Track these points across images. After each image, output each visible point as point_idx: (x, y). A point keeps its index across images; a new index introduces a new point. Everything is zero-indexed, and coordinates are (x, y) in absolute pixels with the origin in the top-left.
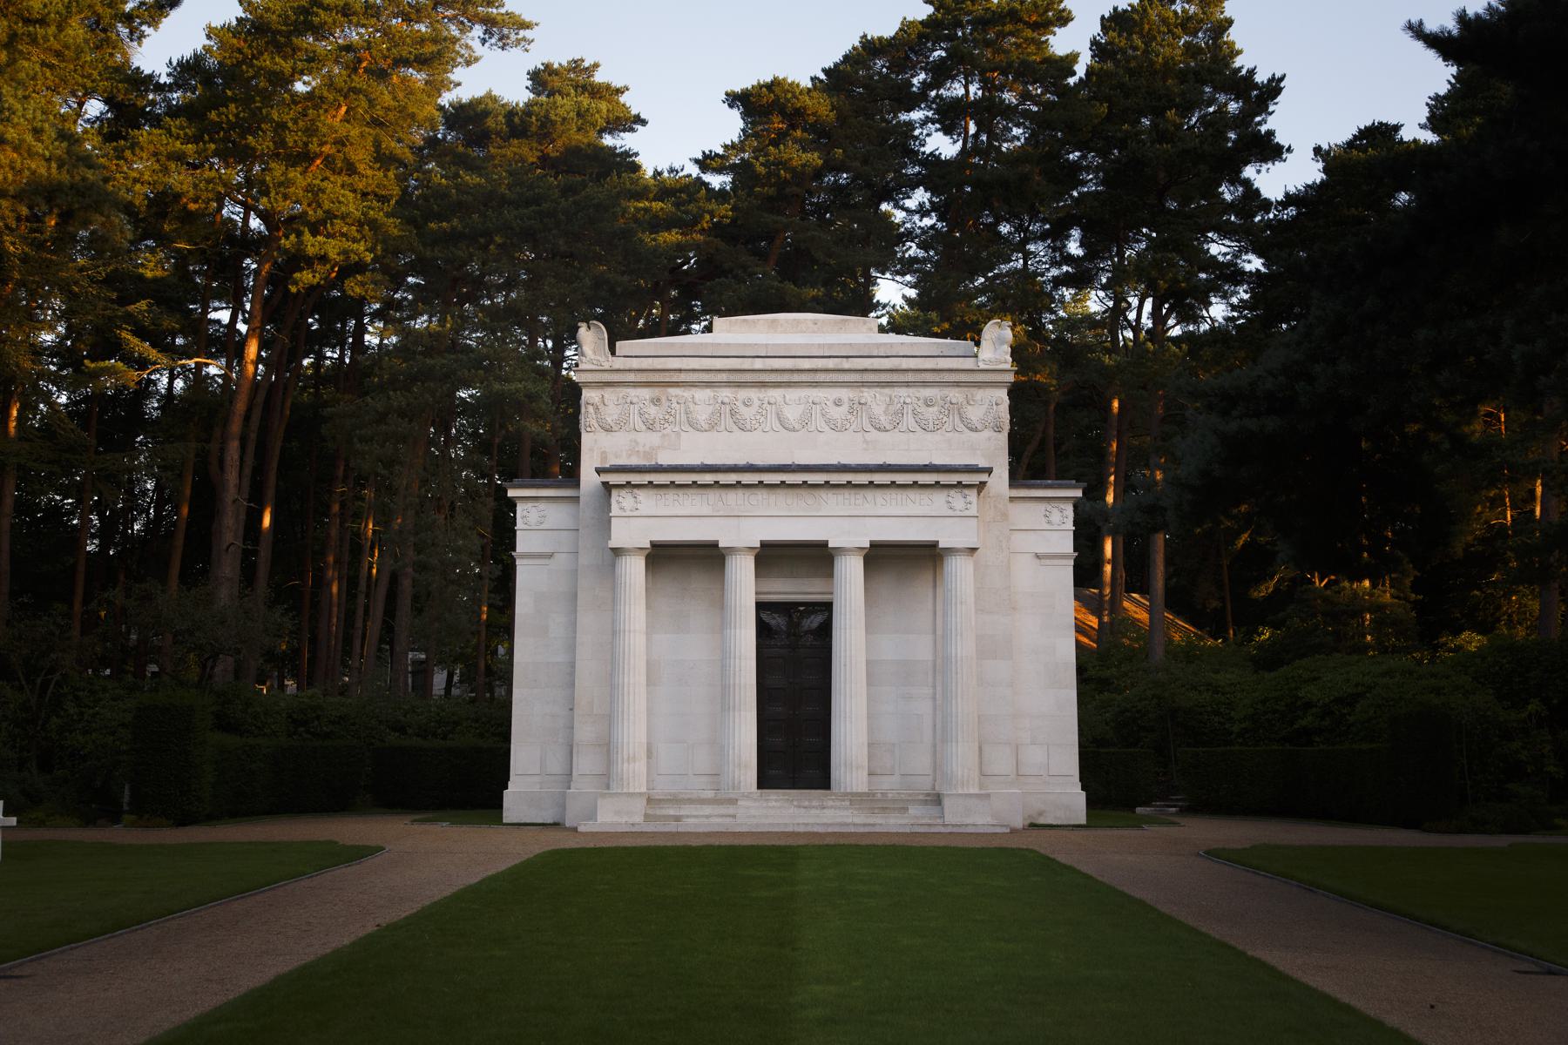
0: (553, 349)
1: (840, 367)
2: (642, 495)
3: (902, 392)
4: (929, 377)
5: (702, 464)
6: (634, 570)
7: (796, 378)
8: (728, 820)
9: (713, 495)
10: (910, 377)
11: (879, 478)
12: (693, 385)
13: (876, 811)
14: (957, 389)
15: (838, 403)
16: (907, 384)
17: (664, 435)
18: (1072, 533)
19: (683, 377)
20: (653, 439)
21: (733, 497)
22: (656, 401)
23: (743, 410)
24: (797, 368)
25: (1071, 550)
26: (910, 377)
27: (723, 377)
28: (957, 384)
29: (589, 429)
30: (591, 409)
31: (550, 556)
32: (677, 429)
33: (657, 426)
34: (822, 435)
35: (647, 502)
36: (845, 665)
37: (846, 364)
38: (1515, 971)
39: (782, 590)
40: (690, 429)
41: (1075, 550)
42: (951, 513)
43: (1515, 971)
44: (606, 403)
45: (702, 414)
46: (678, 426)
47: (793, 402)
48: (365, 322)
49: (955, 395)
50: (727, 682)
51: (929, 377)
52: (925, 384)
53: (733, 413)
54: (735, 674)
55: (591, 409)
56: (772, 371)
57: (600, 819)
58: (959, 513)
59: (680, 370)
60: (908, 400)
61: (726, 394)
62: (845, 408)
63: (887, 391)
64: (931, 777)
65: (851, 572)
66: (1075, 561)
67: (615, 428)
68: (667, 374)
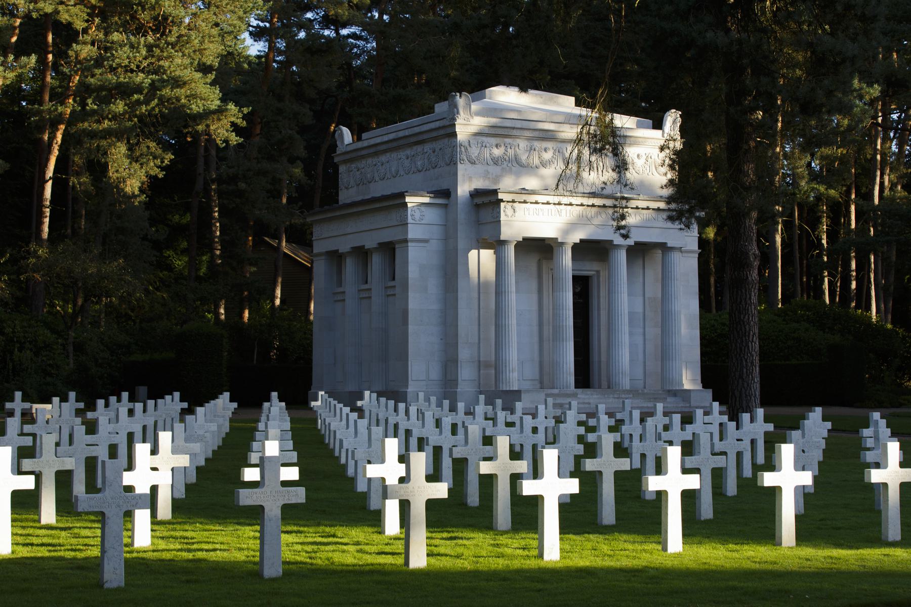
0: (56, 75)
8: (587, 406)
13: (652, 400)
17: (503, 168)
18: (697, 238)
25: (696, 248)
29: (462, 162)
30: (463, 149)
31: (426, 241)
33: (500, 162)
36: (621, 315)
39: (588, 269)
41: (699, 248)
44: (471, 145)
46: (510, 163)
50: (558, 324)
54: (566, 319)
55: (463, 149)
57: (576, 402)
59: (514, 128)
64: (642, 381)
66: (699, 254)
67: (477, 162)
68: (506, 130)
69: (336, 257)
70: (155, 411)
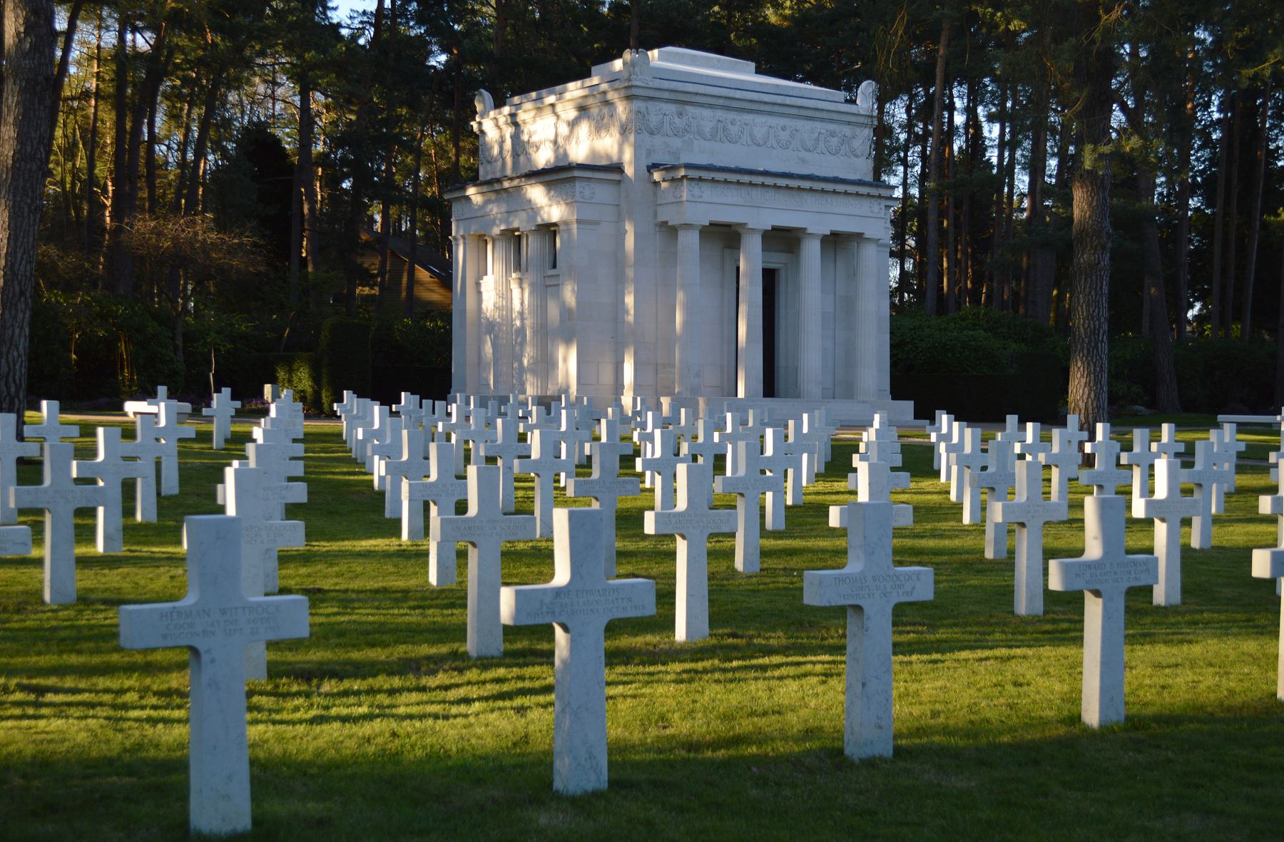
1: (784, 103)
2: (705, 186)
3: (818, 125)
4: (835, 116)
5: (737, 167)
6: (689, 241)
7: (762, 107)
9: (744, 190)
10: (825, 115)
11: (830, 187)
12: (702, 105)
14: (848, 127)
15: (784, 129)
16: (822, 120)
19: (697, 99)
20: (676, 143)
21: (757, 194)
22: (680, 115)
23: (730, 127)
24: (761, 100)
26: (825, 115)
27: (721, 102)
28: (849, 123)
31: (597, 223)
32: (692, 137)
34: (774, 151)
35: (707, 192)
37: (788, 101)
38: (158, 465)
40: (698, 137)
42: (871, 215)
43: (158, 465)
45: (707, 127)
47: (760, 125)
48: (1114, 84)
49: (847, 130)
51: (835, 116)
52: (832, 121)
53: (725, 130)
56: (705, 95)
58: (875, 215)
60: (822, 131)
61: (720, 114)
62: (787, 132)
63: (810, 123)
65: (812, 251)
67: (655, 133)
70: (159, 458)
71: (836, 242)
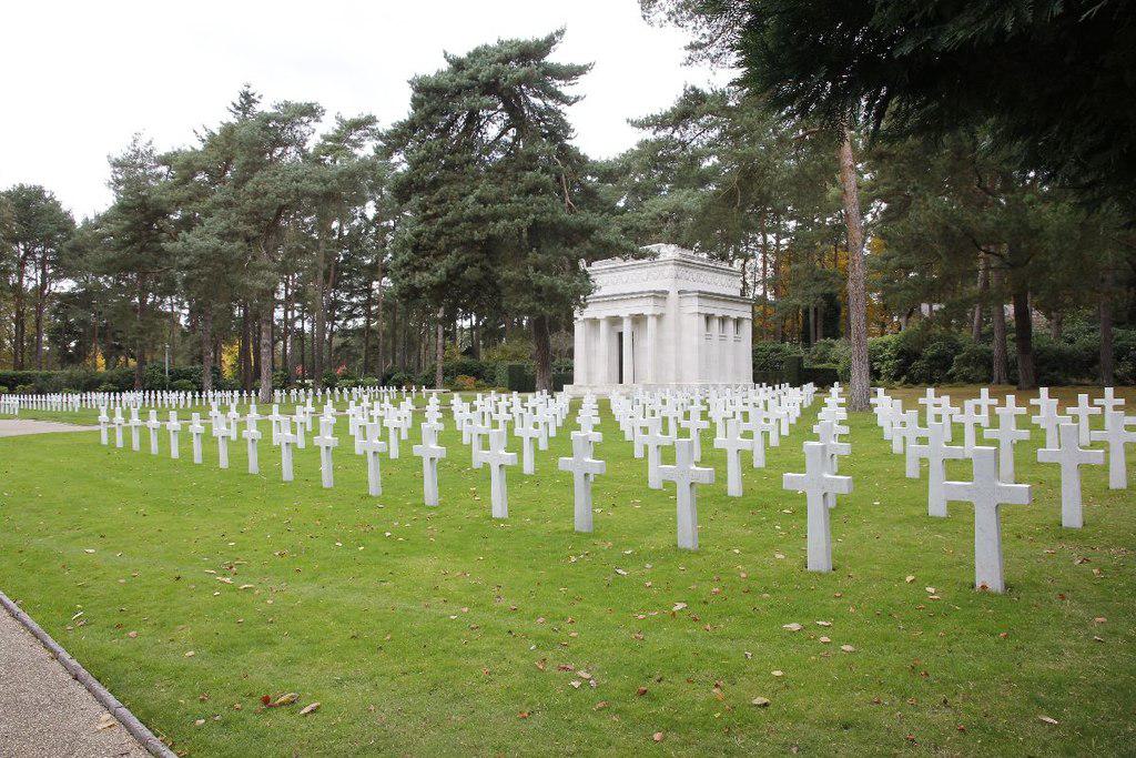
6: (603, 326)
69: (594, 322)
71: (738, 322)
